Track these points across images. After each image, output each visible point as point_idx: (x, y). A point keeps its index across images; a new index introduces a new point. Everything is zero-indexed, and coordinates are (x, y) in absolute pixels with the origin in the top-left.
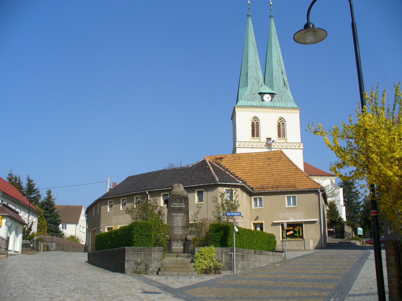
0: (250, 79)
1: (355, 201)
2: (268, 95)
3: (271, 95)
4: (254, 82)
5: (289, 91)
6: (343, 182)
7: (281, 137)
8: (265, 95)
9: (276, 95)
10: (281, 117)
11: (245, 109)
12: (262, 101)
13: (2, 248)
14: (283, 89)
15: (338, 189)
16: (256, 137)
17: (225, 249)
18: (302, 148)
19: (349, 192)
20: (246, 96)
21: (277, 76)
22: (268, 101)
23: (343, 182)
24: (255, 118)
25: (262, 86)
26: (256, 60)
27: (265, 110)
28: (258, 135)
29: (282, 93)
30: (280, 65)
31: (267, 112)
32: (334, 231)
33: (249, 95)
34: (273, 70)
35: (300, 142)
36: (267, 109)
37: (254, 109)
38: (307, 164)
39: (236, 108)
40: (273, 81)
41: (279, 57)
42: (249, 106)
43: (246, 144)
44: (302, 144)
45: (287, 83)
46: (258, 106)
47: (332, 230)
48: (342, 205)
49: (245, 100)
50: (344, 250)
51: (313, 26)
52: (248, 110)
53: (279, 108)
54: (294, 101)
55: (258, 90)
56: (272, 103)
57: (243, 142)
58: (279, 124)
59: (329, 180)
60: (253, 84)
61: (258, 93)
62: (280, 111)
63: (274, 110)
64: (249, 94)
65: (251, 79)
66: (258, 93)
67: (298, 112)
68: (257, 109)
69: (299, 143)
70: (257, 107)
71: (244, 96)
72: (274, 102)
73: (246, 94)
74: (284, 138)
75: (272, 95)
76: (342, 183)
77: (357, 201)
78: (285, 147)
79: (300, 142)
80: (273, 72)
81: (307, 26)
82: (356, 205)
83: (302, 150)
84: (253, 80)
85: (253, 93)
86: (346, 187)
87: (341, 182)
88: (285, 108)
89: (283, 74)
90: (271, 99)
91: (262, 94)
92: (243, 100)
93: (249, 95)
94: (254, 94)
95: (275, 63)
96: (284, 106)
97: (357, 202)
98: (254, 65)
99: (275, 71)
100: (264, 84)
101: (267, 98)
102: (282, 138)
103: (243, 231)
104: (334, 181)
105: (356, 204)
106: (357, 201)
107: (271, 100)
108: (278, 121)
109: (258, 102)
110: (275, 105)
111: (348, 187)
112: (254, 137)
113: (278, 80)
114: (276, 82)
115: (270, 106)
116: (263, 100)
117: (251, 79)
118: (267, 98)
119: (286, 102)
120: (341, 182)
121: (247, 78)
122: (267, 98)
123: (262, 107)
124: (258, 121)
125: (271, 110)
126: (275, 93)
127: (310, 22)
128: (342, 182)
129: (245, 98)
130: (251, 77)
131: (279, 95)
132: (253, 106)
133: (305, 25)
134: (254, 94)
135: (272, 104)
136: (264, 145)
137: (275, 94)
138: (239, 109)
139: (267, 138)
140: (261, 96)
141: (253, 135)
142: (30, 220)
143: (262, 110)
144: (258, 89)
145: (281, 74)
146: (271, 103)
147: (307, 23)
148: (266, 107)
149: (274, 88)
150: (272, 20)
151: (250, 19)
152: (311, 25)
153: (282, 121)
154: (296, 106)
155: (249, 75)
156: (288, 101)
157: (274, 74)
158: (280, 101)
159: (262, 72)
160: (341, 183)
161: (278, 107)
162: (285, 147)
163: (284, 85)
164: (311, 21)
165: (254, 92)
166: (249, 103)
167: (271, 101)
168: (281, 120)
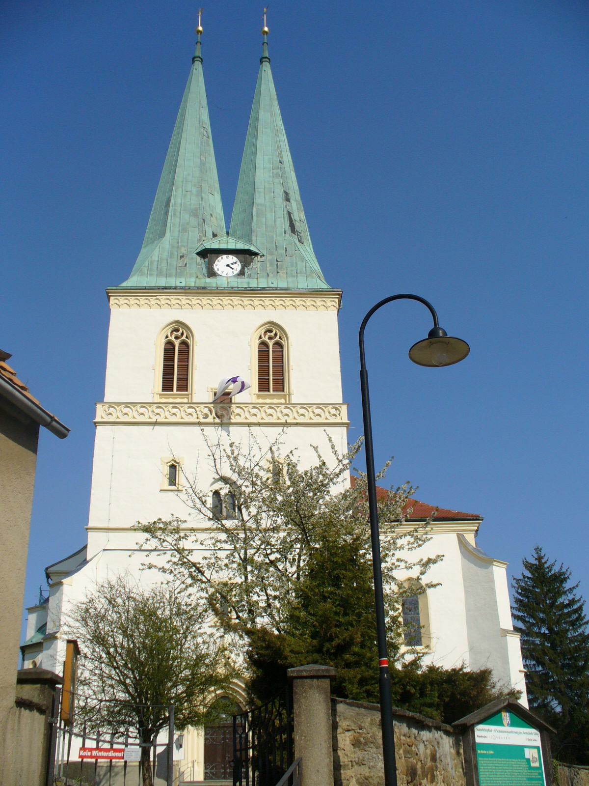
0: (175, 214)
1: (572, 632)
2: (230, 256)
3: (241, 256)
4: (188, 224)
5: (308, 250)
6: (530, 575)
7: (269, 391)
8: (220, 258)
9: (259, 257)
10: (271, 323)
11: (142, 300)
14: (285, 239)
15: (487, 568)
16: (177, 390)
18: (346, 420)
19: (552, 605)
20: (156, 263)
21: (268, 204)
22: (230, 274)
23: (530, 575)
24: (178, 327)
25: (215, 235)
26: (203, 164)
27: (215, 300)
28: (184, 385)
29: (279, 251)
30: (283, 175)
33: (167, 260)
34: (256, 190)
35: (341, 402)
37: (174, 299)
39: (111, 298)
40: (254, 217)
41: (280, 155)
44: (344, 409)
45: (302, 226)
48: (504, 630)
49: (151, 275)
51: (445, 333)
52: (153, 300)
53: (263, 292)
54: (321, 275)
55: (198, 245)
58: (264, 348)
59: (453, 537)
60: (184, 229)
61: (198, 254)
62: (267, 301)
63: (246, 301)
64: (165, 255)
65: (178, 214)
66: (198, 254)
67: (332, 303)
68: (184, 299)
71: (146, 263)
72: (249, 276)
73: (155, 258)
74: (283, 391)
75: (246, 255)
76: (528, 578)
77: (580, 631)
79: (341, 402)
80: (256, 195)
81: (433, 334)
82: (576, 644)
83: (344, 430)
86: (542, 590)
87: (524, 577)
89: (288, 200)
91: (209, 254)
92: (143, 274)
93: (167, 260)
94: (182, 257)
95: (262, 171)
96: (283, 284)
97: (580, 635)
98: (192, 177)
99: (262, 190)
100: (228, 233)
101: (226, 266)
103: (69, 765)
104: (470, 538)
105: (576, 641)
106: (580, 631)
107: (242, 273)
108: (260, 338)
111: (545, 589)
112: (172, 390)
113: (270, 216)
114: (264, 220)
116: (212, 273)
117: (178, 214)
118: (228, 265)
119: (293, 276)
120: (524, 577)
121: (166, 213)
122: (226, 266)
124: (187, 337)
125: (236, 300)
126: (253, 248)
127: (439, 328)
128: (527, 577)
129: (151, 270)
130: (179, 210)
131: (269, 257)
133: (430, 332)
134: (182, 257)
135: (243, 282)
137: (256, 254)
138: (122, 300)
140: (206, 260)
141: (167, 385)
143: (205, 300)
144: (199, 242)
145: (280, 200)
147: (434, 328)
148: (218, 291)
149: (254, 238)
150: (266, 68)
151: (198, 65)
152: (441, 332)
154: (324, 286)
155: (175, 204)
156: (299, 275)
157: (259, 199)
158: (271, 275)
160: (526, 579)
161: (263, 288)
163: (288, 228)
164: (441, 324)
165: (183, 251)
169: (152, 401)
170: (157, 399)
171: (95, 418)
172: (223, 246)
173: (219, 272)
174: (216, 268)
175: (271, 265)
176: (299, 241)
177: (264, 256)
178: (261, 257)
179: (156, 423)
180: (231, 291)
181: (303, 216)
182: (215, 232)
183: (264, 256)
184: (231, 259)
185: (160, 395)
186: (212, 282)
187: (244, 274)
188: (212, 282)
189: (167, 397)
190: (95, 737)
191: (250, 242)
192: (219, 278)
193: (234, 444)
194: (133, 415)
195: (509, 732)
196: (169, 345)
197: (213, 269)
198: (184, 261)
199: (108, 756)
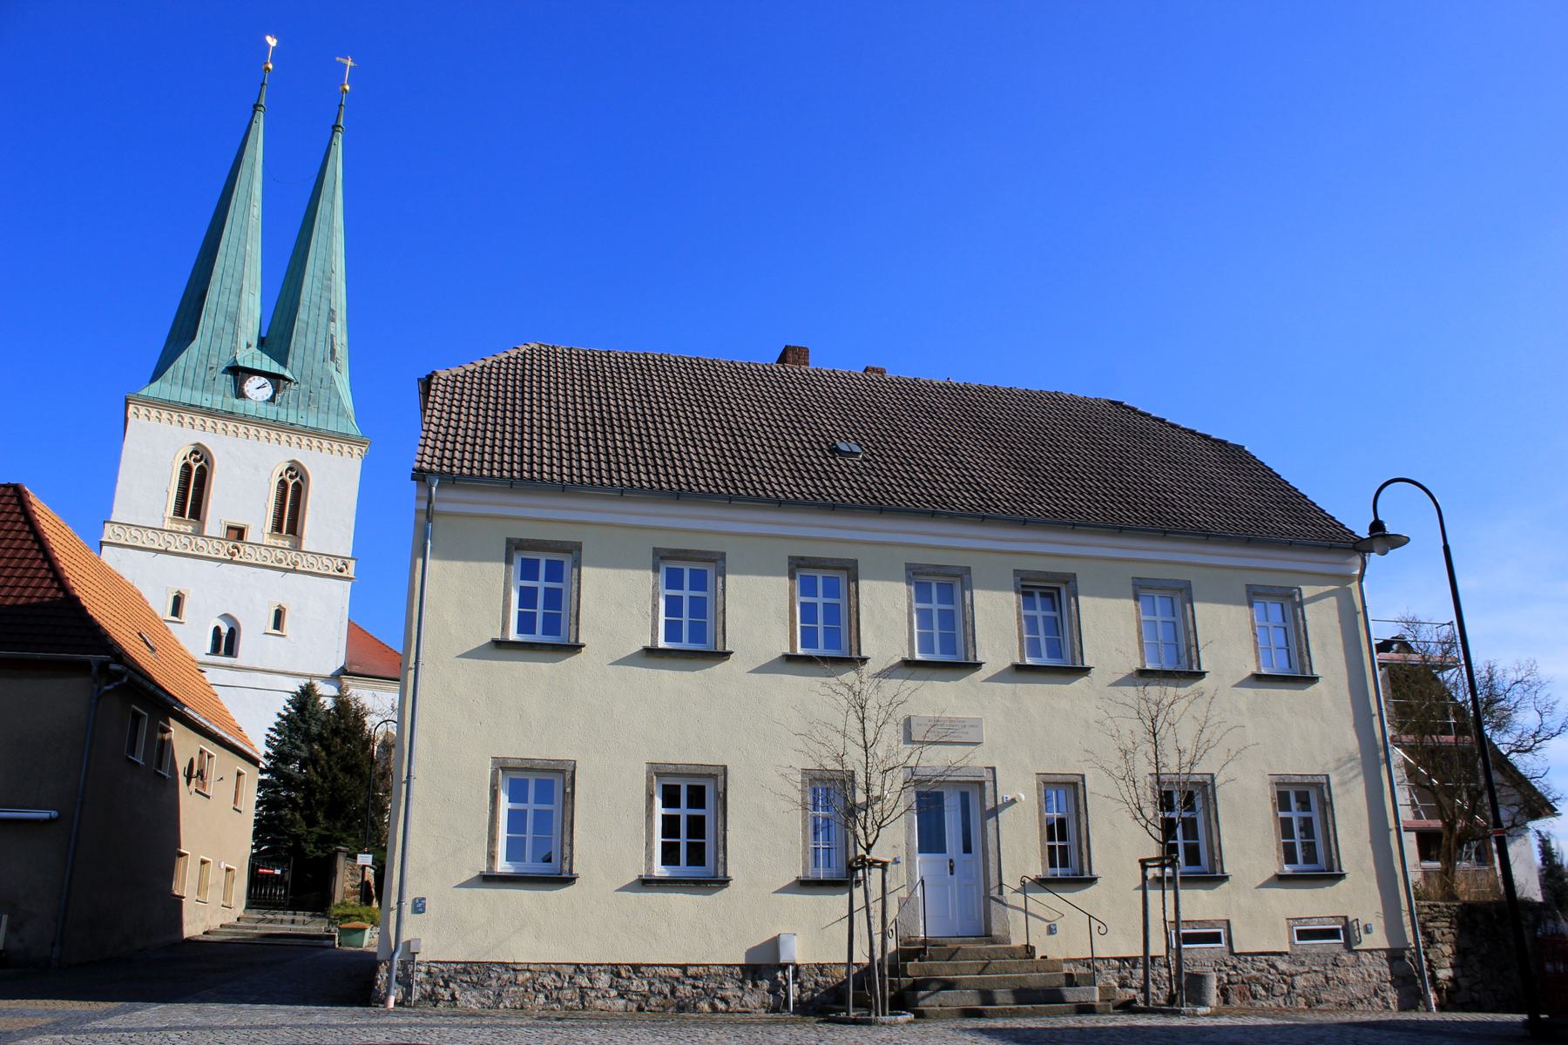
3: (275, 381)
12: (237, 398)
13: (1131, 987)
17: (286, 1011)
24: (200, 452)
31: (202, 429)
32: (287, 877)
36: (249, 427)
38: (353, 623)
42: (184, 404)
43: (305, 560)
46: (217, 410)
47: (278, 872)
50: (1201, 851)
53: (291, 428)
56: (273, 408)
57: (309, 555)
69: (219, 538)
70: (210, 413)
72: (280, 405)
78: (288, 564)
79: (350, 556)
84: (221, 319)
85: (209, 366)
88: (315, 432)
90: (270, 395)
91: (239, 373)
94: (211, 368)
96: (312, 423)
101: (257, 389)
102: (1376, 657)
107: (272, 399)
109: (220, 398)
110: (282, 417)
115: (261, 418)
116: (240, 394)
122: (257, 389)
123: (230, 415)
126: (287, 374)
132: (196, 406)
134: (211, 368)
135: (271, 412)
136: (335, 565)
137: (290, 381)
139: (229, 528)
142: (1410, 841)
146: (269, 408)
148: (245, 419)
153: (202, 457)
154: (354, 430)
159: (262, 304)
161: (291, 424)
162: (288, 564)
166: (186, 396)
167: (268, 401)
168: (198, 457)
169: (1398, 803)
170: (168, 525)
171: (102, 536)
172: (257, 366)
173: (248, 394)
174: (246, 389)
175: (304, 396)
176: (337, 370)
177: (297, 383)
178: (295, 384)
179: (166, 552)
180: (260, 422)
181: (345, 339)
182: (249, 343)
183: (297, 383)
184: (263, 380)
185: (172, 519)
186: (239, 406)
187: (274, 402)
188: (239, 406)
189: (179, 522)
190: (1162, 777)
191: (284, 363)
192: (247, 401)
193: (1542, 825)
194: (144, 539)
195: (1085, 791)
196: (187, 468)
197: (243, 389)
198: (212, 374)
199: (51, 817)
